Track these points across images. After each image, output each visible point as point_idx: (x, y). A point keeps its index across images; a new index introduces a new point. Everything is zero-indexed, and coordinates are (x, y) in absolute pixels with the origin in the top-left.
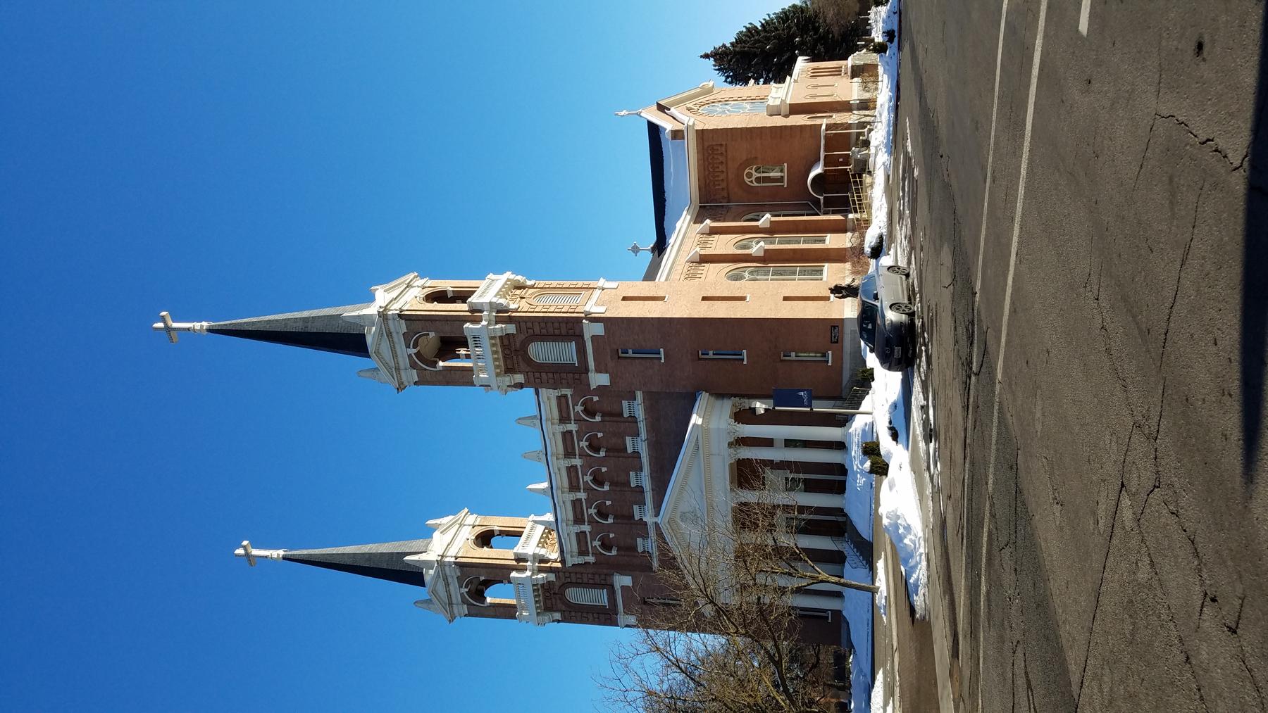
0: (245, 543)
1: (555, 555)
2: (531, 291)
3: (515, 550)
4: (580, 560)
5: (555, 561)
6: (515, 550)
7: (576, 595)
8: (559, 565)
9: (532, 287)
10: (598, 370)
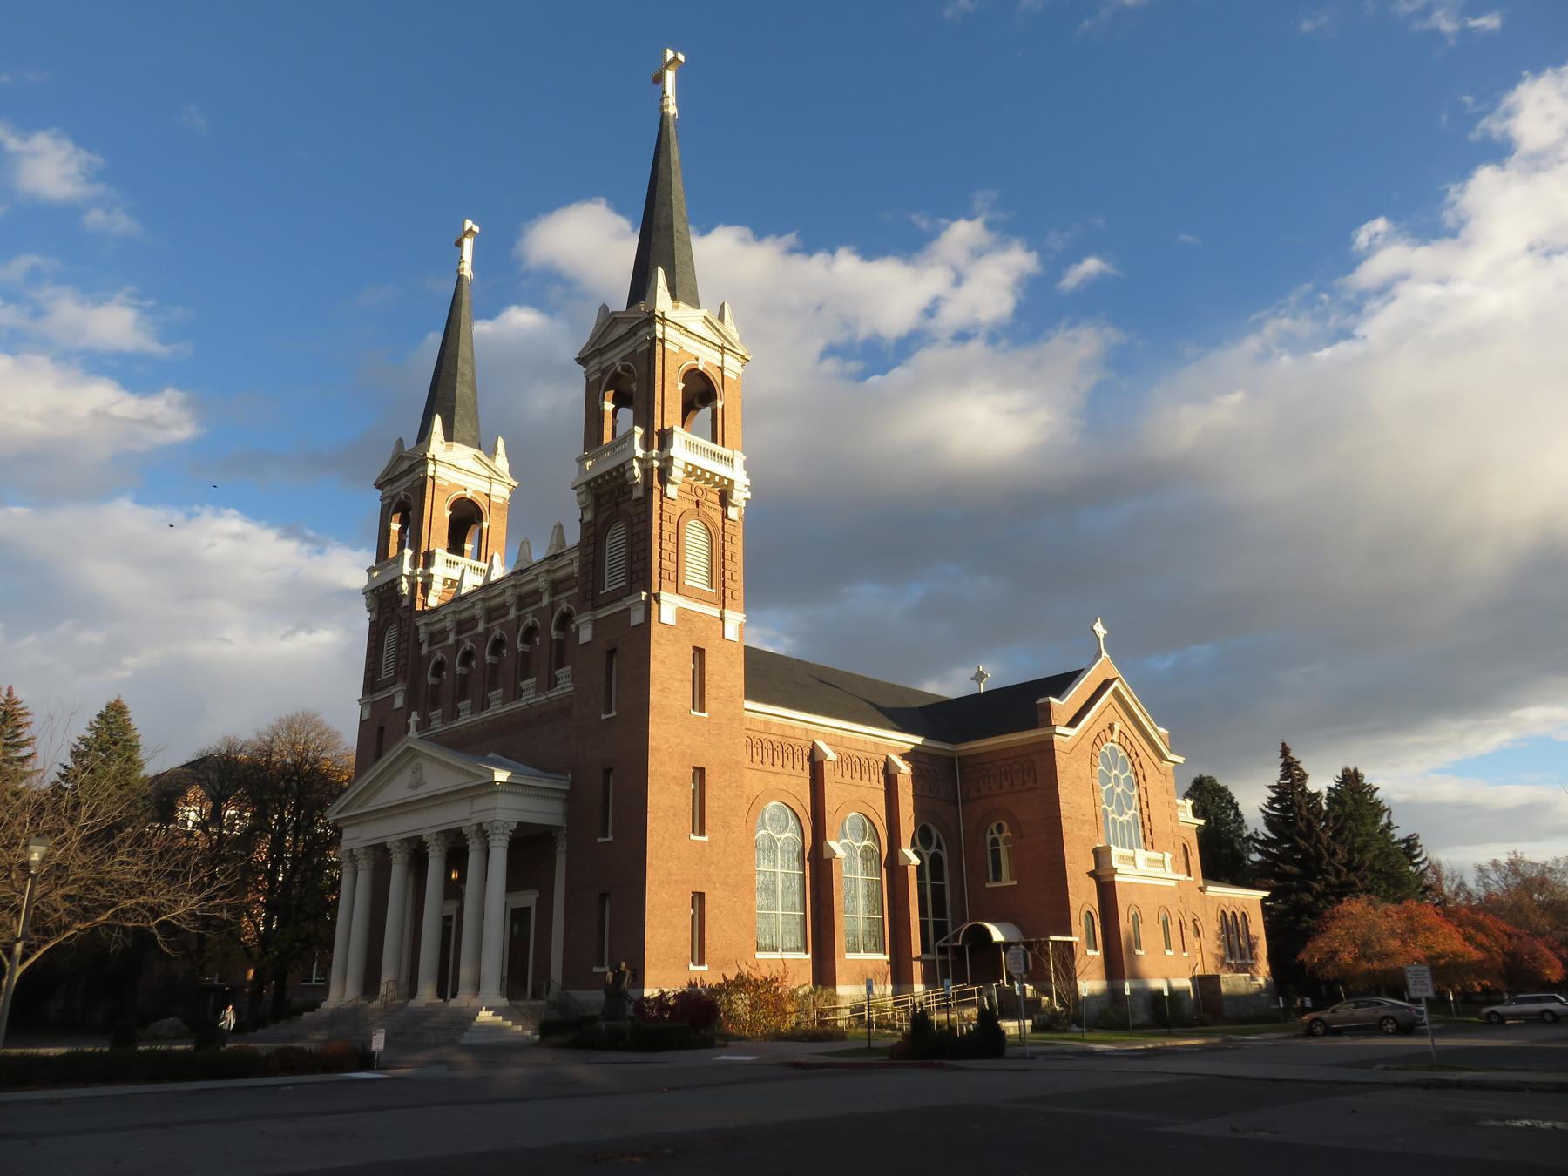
0: (681, 57)
1: (433, 602)
2: (718, 517)
3: (678, 429)
4: (423, 636)
5: (425, 604)
6: (678, 429)
7: (391, 635)
8: (419, 607)
9: (725, 516)
10: (596, 624)
